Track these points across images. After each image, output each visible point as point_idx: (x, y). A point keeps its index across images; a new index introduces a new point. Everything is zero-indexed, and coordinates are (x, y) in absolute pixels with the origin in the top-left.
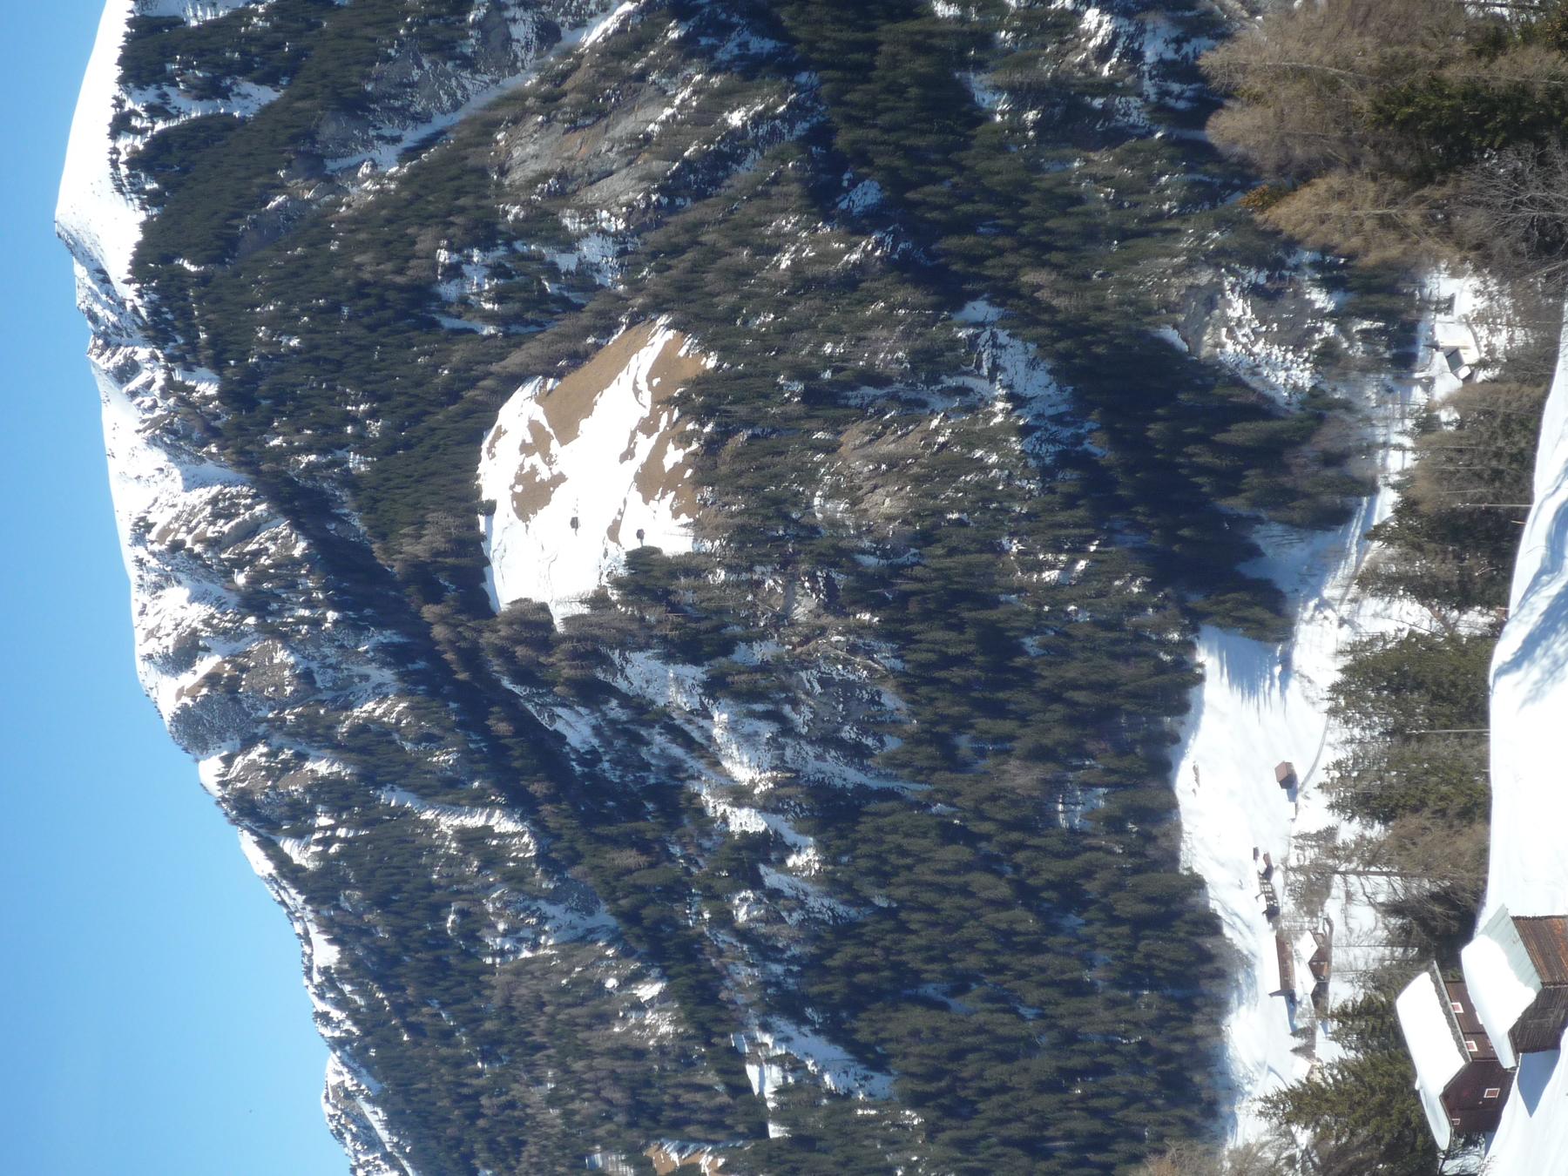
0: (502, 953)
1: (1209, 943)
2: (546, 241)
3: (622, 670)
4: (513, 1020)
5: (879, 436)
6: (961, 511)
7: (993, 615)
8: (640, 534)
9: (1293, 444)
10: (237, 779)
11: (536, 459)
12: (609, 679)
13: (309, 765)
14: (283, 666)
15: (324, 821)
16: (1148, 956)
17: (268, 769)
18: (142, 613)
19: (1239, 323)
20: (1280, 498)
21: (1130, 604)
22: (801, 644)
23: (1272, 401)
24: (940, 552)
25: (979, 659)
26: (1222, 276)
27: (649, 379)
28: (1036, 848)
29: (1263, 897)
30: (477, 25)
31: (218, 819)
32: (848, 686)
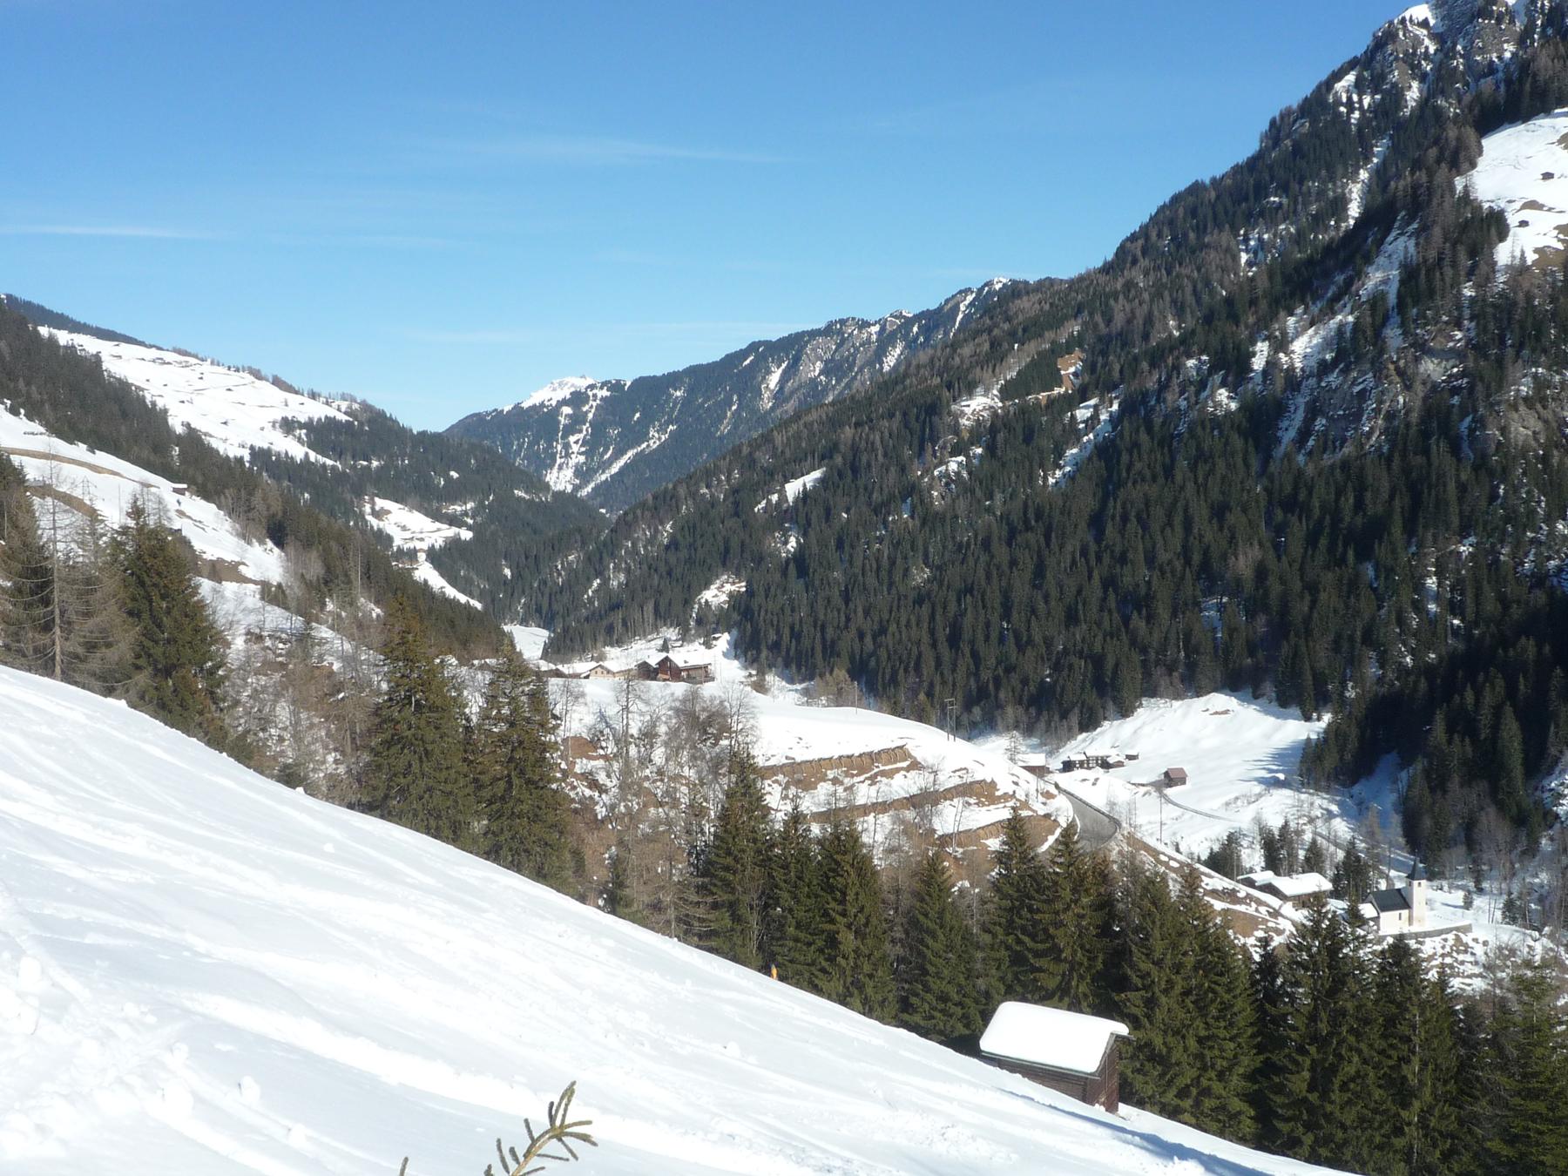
0: (1246, 240)
1: (1074, 719)
3: (1402, 234)
4: (1193, 252)
7: (1397, 530)
8: (1524, 224)
9: (1494, 791)
12: (1397, 224)
13: (1415, 84)
14: (1501, 52)
16: (1071, 666)
17: (1414, 53)
20: (1437, 782)
21: (1385, 651)
22: (1397, 369)
23: (1550, 773)
24: (1464, 477)
25: (1359, 520)
28: (1183, 578)
29: (1083, 758)
31: (1378, 25)
32: (1357, 417)
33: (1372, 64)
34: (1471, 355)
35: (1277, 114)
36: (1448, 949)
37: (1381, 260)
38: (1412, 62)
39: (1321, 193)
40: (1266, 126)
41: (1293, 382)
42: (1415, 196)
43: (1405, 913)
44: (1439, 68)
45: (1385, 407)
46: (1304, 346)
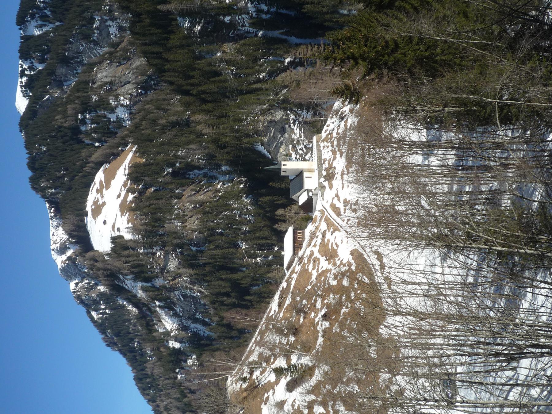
2: (105, 109)
3: (124, 282)
4: (154, 379)
5: (198, 192)
6: (221, 229)
7: (236, 276)
10: (78, 291)
11: (99, 196)
13: (99, 288)
15: (102, 307)
18: (53, 235)
19: (298, 143)
22: (172, 280)
26: (288, 114)
27: (129, 164)
30: (97, 28)
31: (75, 302)
33: (89, 305)
34: (167, 248)
35: (105, 344)
36: (329, 144)
37: (134, 291)
38: (90, 289)
39: (135, 325)
40: (109, 348)
41: (183, 328)
42: (108, 276)
43: (305, 174)
44: (93, 278)
45: (189, 286)
46: (169, 324)
